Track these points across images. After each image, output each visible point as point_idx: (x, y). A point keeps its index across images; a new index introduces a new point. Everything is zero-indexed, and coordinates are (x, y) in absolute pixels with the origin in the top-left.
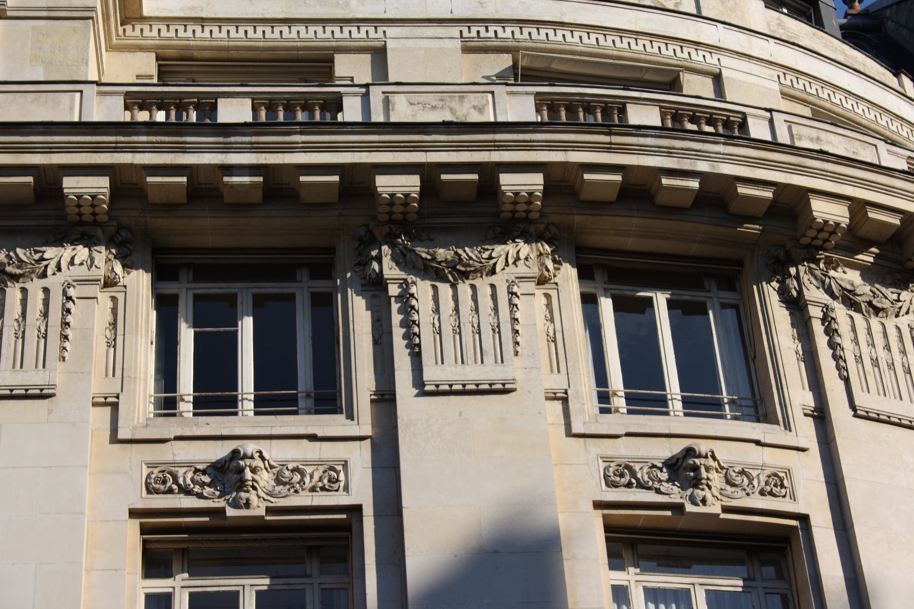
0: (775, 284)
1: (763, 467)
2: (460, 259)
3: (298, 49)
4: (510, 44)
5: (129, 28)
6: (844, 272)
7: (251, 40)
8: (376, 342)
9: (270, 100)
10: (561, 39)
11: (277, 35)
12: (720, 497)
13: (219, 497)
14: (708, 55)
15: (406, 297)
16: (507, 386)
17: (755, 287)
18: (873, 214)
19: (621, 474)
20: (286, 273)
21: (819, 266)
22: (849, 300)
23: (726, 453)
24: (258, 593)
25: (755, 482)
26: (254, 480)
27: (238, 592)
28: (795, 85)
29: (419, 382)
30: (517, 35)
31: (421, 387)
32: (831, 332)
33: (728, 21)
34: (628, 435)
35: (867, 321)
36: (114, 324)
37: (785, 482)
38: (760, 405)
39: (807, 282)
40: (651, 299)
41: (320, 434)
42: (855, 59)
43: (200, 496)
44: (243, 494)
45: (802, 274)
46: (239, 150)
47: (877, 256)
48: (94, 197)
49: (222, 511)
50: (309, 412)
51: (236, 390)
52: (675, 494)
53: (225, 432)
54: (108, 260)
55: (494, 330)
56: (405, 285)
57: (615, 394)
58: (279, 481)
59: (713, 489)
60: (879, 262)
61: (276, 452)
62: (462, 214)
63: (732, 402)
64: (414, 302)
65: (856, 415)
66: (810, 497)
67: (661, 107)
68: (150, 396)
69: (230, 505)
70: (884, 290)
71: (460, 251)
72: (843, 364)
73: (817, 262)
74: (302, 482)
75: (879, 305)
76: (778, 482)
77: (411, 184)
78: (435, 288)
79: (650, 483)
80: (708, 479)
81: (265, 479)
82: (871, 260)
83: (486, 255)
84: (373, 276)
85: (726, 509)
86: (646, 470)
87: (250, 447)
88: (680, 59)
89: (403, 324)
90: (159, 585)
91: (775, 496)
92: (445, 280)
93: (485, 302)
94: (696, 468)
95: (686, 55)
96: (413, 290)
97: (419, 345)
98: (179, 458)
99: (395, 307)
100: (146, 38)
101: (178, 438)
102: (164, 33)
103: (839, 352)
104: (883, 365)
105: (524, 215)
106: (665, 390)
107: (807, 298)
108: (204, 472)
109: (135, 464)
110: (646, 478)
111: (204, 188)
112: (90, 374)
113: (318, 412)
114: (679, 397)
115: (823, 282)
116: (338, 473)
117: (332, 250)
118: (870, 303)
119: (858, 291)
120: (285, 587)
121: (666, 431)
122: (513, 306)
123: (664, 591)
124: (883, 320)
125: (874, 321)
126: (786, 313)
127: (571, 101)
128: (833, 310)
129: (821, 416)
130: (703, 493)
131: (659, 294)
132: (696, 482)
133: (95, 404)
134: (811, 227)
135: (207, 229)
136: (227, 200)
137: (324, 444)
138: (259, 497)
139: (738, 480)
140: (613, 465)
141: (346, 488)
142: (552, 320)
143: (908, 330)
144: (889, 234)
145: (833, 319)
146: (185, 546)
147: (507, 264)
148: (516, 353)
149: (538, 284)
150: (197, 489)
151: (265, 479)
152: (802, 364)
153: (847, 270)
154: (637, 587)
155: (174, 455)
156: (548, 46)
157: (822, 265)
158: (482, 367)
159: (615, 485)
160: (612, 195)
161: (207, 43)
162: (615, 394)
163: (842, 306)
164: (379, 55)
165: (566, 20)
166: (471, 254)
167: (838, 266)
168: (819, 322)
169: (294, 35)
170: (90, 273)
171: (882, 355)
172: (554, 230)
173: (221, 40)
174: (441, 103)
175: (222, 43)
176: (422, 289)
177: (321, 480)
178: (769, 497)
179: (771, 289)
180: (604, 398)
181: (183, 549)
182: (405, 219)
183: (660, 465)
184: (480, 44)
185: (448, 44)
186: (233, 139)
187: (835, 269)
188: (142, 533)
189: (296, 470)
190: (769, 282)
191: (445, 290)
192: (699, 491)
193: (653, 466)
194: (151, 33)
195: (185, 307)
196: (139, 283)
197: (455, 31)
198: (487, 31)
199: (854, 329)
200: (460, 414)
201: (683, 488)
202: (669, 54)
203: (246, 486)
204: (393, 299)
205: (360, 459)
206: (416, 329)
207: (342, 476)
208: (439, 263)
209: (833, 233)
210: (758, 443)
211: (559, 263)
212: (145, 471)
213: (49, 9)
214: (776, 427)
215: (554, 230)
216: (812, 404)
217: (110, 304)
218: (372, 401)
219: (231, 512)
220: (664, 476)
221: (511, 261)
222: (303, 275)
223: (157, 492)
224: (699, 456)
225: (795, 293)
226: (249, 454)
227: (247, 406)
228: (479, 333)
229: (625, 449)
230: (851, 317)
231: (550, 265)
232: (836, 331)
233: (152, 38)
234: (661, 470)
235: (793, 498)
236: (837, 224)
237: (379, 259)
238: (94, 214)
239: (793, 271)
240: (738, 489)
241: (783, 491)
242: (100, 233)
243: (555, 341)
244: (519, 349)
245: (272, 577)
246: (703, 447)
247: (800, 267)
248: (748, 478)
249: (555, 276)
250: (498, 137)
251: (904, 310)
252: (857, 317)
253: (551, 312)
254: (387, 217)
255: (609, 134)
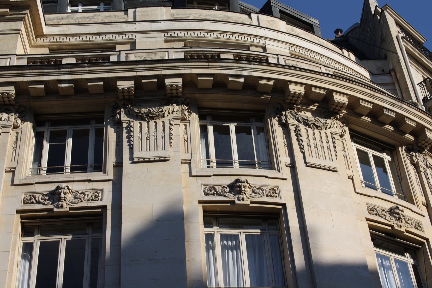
0: (277, 118)
1: (268, 186)
2: (150, 112)
3: (102, 44)
4: (183, 38)
5: (39, 39)
6: (305, 113)
7: (84, 41)
8: (117, 145)
9: (83, 58)
10: (203, 36)
11: (94, 39)
12: (249, 197)
13: (51, 204)
14: (261, 40)
15: (129, 128)
16: (166, 158)
17: (269, 120)
18: (314, 90)
19: (211, 190)
20: (87, 122)
21: (294, 111)
22: (306, 123)
23: (252, 181)
24: (67, 241)
25: (264, 192)
26: (65, 197)
27: (59, 241)
28: (296, 50)
29: (132, 158)
30: (186, 35)
31: (133, 160)
32: (298, 135)
33: (269, 27)
34: (214, 175)
35: (313, 131)
36: (16, 142)
37: (277, 192)
38: (270, 163)
39: (289, 117)
40: (229, 126)
41: (92, 179)
42: (323, 43)
43: (44, 204)
44: (60, 203)
45: (287, 114)
46: (64, 74)
47: (318, 107)
48: (8, 94)
49: (53, 209)
50: (91, 172)
51: (64, 165)
52: (232, 197)
53: (55, 180)
54: (15, 118)
55: (162, 138)
56: (129, 123)
57: (212, 161)
58: (75, 198)
59: (247, 194)
60: (319, 109)
61: (74, 187)
62: (151, 96)
63: (259, 163)
64: (132, 129)
65: (307, 166)
66: (287, 196)
67: (234, 55)
68: (30, 169)
69: (55, 207)
70: (320, 119)
71: (151, 109)
72: (302, 147)
73: (293, 109)
74: (84, 197)
75: (318, 125)
76: (274, 192)
77: (131, 84)
78: (140, 123)
79: (222, 193)
80: (245, 191)
81: (70, 197)
82: (316, 108)
83: (160, 110)
84: (117, 120)
85: (252, 202)
86: (220, 188)
87: (64, 185)
88: (249, 42)
89: (128, 137)
90: (28, 239)
91: (272, 197)
92: (144, 120)
93: (160, 128)
94: (240, 187)
95: (252, 40)
96: (132, 124)
97: (133, 145)
98: (37, 190)
99: (125, 131)
100: (45, 42)
101: (37, 183)
102: (52, 40)
103: (301, 142)
104: (319, 147)
105: (176, 94)
106: (232, 159)
107: (289, 122)
108: (46, 195)
109: (20, 194)
110: (220, 191)
111: (51, 89)
112: (4, 160)
113: (94, 172)
114: (238, 162)
115: (295, 117)
116: (98, 193)
117: (103, 112)
118: (314, 124)
119: (309, 120)
120: (78, 239)
121: (229, 174)
122: (170, 128)
123: (231, 235)
124: (320, 131)
125: (316, 131)
126: (281, 129)
127: (199, 54)
128: (299, 127)
129: (293, 167)
130: (243, 196)
131: (232, 124)
132: (240, 192)
133: (6, 172)
134: (289, 96)
135: (54, 106)
136: (61, 94)
137: (94, 183)
138: (67, 204)
139: (257, 191)
140: (207, 187)
141: (101, 199)
142: (187, 134)
143: (330, 134)
144: (322, 98)
145: (299, 130)
146: (39, 224)
147: (169, 113)
148: (171, 146)
149: (182, 121)
150: (43, 201)
151: (70, 197)
152: (286, 148)
153: (306, 112)
154: (217, 234)
155: (35, 189)
156: (198, 38)
157: (295, 111)
158: (157, 152)
159: (208, 194)
160: (210, 86)
161: (68, 43)
162: (212, 161)
163: (303, 125)
164: (133, 44)
165: (205, 29)
166: (154, 110)
167: (302, 111)
168: (294, 131)
169: (101, 39)
170: (8, 123)
171: (319, 143)
172: (188, 100)
173: (73, 42)
174: (147, 56)
175: (73, 43)
176: (136, 124)
177: (92, 196)
178: (270, 197)
179: (275, 120)
180: (208, 163)
181: (39, 225)
182: (130, 98)
183: (226, 186)
184: (172, 39)
185: (159, 39)
186: (62, 70)
187: (301, 112)
188: (21, 219)
189: (82, 193)
190: (274, 118)
191: (144, 124)
192: (241, 196)
193: (224, 187)
194: (47, 40)
195: (47, 135)
196: (28, 127)
197: (162, 35)
198: (174, 34)
199: (308, 134)
200: (147, 169)
201: (235, 195)
202: (245, 40)
203: (62, 200)
204: (124, 128)
205: (108, 188)
206: (132, 139)
207: (100, 195)
208: (142, 114)
209: (298, 97)
210: (266, 177)
211: (191, 113)
212: (24, 196)
213: (3, 31)
214: (274, 171)
215: (188, 100)
216: (290, 162)
217: (15, 135)
218: (114, 166)
219: (55, 210)
220: (228, 190)
221: (170, 112)
222: (93, 122)
223: (27, 203)
224: (241, 182)
225: (284, 121)
226: (63, 187)
227: (68, 171)
228: (157, 139)
229: (212, 181)
230: (307, 130)
231: (187, 113)
232: (300, 134)
233: (47, 42)
234: (226, 188)
235: (280, 197)
236: (300, 94)
237: (120, 114)
238: (9, 101)
239: (284, 113)
240: (258, 195)
241: (276, 195)
242: (12, 108)
243: (187, 142)
244: (172, 144)
245: (73, 235)
246: (243, 179)
247: (287, 112)
248: (262, 190)
249: (189, 118)
250: (164, 65)
251: (328, 127)
252: (309, 129)
253: (187, 131)
254: (122, 98)
255: (208, 62)
